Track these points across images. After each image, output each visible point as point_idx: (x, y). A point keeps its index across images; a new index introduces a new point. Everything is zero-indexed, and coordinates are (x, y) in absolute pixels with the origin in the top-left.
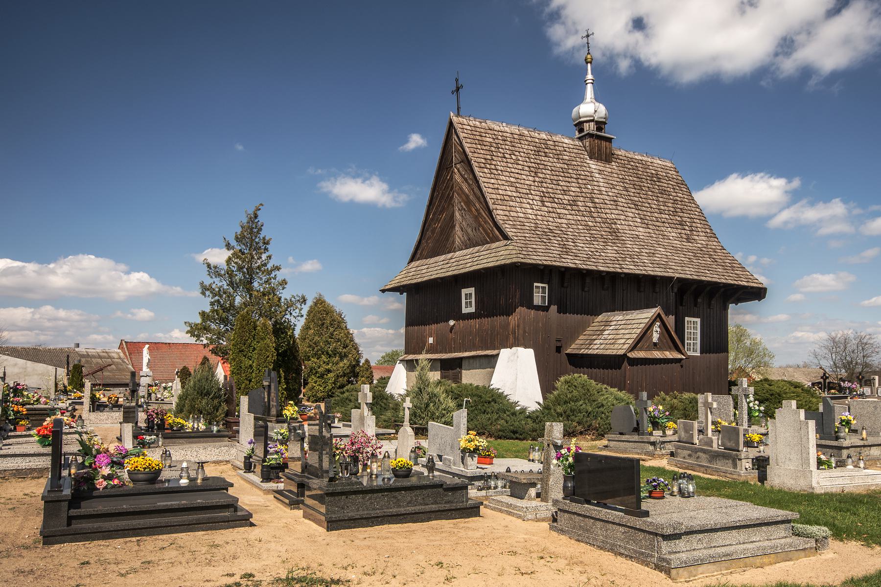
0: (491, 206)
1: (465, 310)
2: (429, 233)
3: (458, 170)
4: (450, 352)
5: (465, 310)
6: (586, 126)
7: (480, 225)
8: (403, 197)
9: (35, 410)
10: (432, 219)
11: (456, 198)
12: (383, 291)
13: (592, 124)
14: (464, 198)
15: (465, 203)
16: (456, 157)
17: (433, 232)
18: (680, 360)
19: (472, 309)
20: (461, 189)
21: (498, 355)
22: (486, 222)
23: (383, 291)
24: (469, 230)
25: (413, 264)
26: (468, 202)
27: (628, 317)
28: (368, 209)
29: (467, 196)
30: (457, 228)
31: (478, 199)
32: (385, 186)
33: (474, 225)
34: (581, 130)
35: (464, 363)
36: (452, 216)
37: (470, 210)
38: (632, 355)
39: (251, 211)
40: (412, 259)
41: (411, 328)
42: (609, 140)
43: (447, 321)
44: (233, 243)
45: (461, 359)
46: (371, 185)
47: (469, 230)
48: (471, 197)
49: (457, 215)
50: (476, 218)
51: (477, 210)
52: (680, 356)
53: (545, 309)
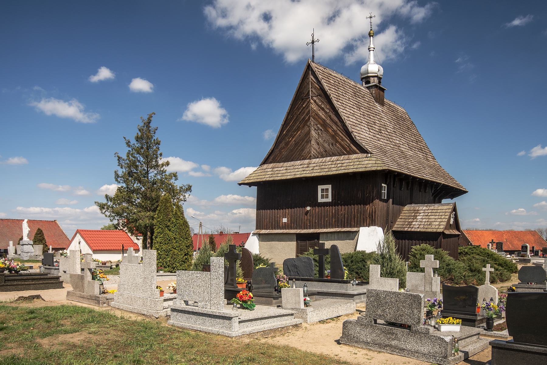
0: (350, 130)
1: (320, 200)
2: (282, 145)
3: (315, 101)
4: (301, 228)
5: (320, 200)
6: (372, 79)
7: (337, 141)
8: (96, 116)
9: (31, 275)
10: (286, 135)
11: (312, 121)
12: (240, 184)
13: (376, 79)
14: (321, 122)
15: (321, 125)
16: (312, 91)
17: (287, 144)
18: (459, 235)
19: (329, 200)
20: (317, 115)
21: (357, 232)
22: (343, 140)
23: (240, 184)
24: (326, 145)
25: (265, 166)
26: (325, 125)
27: (432, 208)
28: (68, 122)
29: (324, 121)
30: (313, 142)
31: (336, 123)
32: (82, 107)
33: (331, 141)
34: (368, 82)
35: (321, 236)
36: (309, 132)
37: (327, 131)
38: (447, 232)
39: (146, 118)
40: (265, 162)
41: (263, 212)
42: (383, 90)
43: (305, 206)
44: (133, 141)
45: (319, 233)
46: (70, 105)
47: (326, 145)
48: (328, 121)
49: (313, 133)
50: (333, 137)
51: (334, 131)
52: (457, 233)
53: (386, 201)
